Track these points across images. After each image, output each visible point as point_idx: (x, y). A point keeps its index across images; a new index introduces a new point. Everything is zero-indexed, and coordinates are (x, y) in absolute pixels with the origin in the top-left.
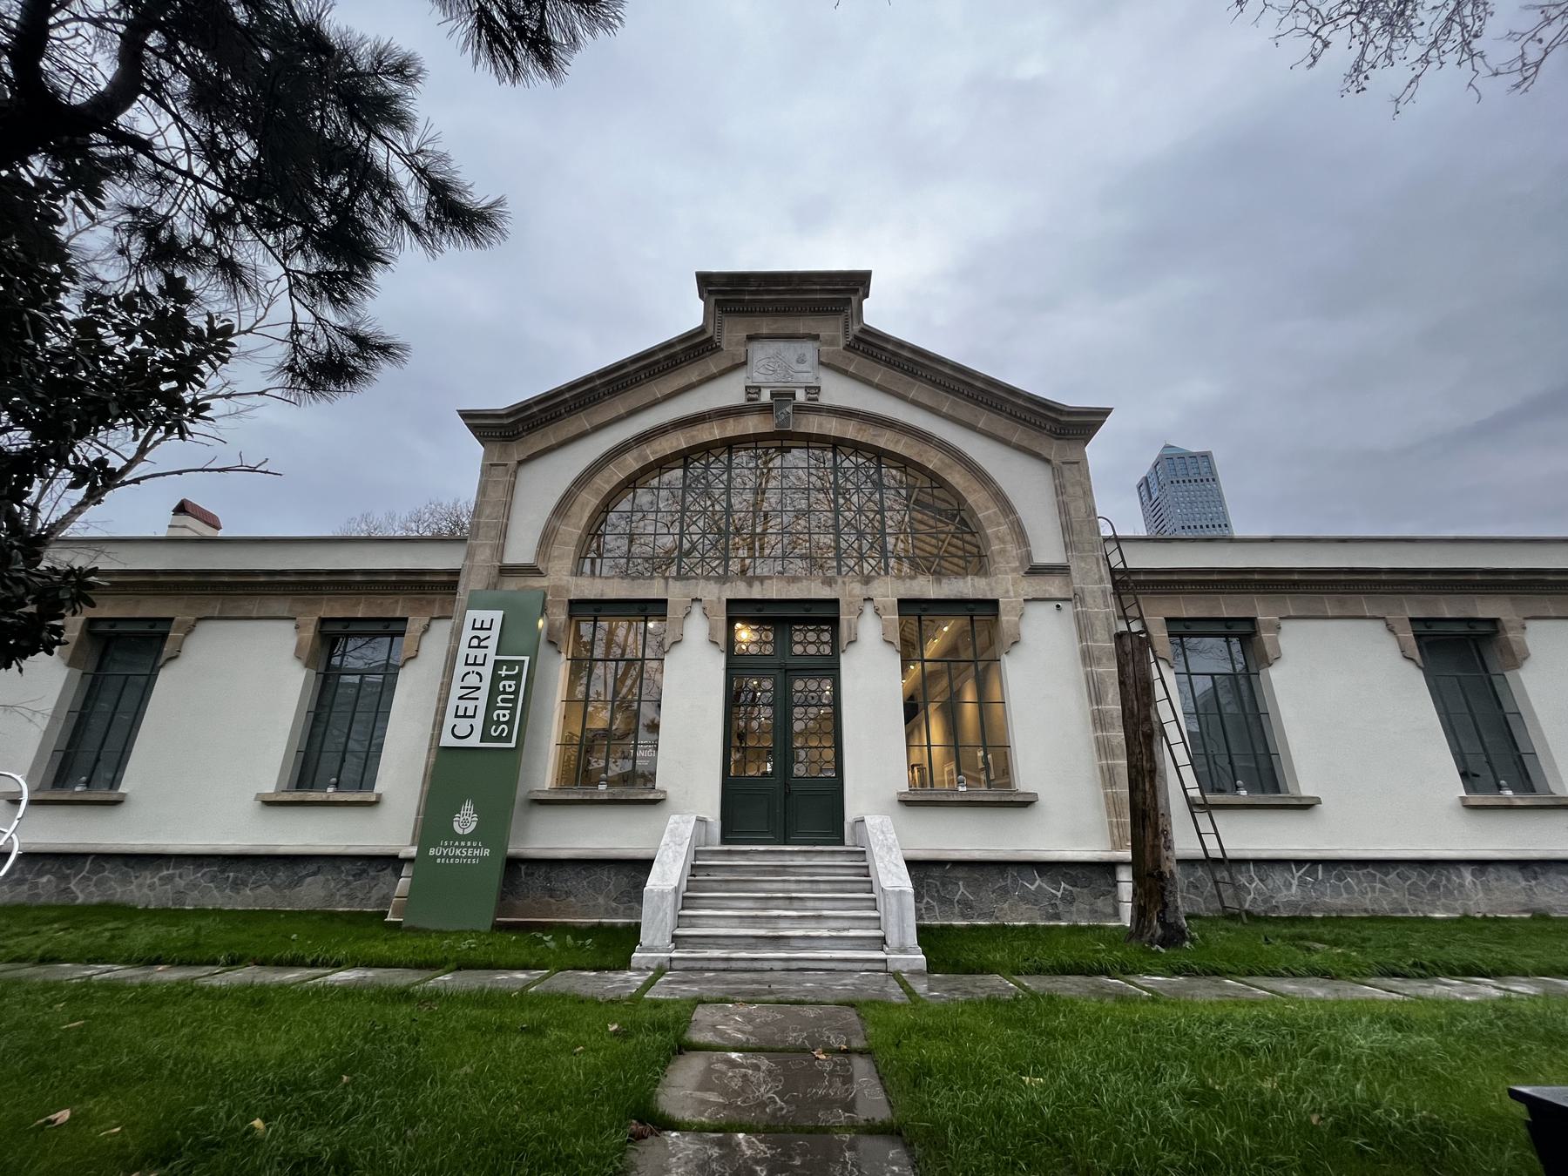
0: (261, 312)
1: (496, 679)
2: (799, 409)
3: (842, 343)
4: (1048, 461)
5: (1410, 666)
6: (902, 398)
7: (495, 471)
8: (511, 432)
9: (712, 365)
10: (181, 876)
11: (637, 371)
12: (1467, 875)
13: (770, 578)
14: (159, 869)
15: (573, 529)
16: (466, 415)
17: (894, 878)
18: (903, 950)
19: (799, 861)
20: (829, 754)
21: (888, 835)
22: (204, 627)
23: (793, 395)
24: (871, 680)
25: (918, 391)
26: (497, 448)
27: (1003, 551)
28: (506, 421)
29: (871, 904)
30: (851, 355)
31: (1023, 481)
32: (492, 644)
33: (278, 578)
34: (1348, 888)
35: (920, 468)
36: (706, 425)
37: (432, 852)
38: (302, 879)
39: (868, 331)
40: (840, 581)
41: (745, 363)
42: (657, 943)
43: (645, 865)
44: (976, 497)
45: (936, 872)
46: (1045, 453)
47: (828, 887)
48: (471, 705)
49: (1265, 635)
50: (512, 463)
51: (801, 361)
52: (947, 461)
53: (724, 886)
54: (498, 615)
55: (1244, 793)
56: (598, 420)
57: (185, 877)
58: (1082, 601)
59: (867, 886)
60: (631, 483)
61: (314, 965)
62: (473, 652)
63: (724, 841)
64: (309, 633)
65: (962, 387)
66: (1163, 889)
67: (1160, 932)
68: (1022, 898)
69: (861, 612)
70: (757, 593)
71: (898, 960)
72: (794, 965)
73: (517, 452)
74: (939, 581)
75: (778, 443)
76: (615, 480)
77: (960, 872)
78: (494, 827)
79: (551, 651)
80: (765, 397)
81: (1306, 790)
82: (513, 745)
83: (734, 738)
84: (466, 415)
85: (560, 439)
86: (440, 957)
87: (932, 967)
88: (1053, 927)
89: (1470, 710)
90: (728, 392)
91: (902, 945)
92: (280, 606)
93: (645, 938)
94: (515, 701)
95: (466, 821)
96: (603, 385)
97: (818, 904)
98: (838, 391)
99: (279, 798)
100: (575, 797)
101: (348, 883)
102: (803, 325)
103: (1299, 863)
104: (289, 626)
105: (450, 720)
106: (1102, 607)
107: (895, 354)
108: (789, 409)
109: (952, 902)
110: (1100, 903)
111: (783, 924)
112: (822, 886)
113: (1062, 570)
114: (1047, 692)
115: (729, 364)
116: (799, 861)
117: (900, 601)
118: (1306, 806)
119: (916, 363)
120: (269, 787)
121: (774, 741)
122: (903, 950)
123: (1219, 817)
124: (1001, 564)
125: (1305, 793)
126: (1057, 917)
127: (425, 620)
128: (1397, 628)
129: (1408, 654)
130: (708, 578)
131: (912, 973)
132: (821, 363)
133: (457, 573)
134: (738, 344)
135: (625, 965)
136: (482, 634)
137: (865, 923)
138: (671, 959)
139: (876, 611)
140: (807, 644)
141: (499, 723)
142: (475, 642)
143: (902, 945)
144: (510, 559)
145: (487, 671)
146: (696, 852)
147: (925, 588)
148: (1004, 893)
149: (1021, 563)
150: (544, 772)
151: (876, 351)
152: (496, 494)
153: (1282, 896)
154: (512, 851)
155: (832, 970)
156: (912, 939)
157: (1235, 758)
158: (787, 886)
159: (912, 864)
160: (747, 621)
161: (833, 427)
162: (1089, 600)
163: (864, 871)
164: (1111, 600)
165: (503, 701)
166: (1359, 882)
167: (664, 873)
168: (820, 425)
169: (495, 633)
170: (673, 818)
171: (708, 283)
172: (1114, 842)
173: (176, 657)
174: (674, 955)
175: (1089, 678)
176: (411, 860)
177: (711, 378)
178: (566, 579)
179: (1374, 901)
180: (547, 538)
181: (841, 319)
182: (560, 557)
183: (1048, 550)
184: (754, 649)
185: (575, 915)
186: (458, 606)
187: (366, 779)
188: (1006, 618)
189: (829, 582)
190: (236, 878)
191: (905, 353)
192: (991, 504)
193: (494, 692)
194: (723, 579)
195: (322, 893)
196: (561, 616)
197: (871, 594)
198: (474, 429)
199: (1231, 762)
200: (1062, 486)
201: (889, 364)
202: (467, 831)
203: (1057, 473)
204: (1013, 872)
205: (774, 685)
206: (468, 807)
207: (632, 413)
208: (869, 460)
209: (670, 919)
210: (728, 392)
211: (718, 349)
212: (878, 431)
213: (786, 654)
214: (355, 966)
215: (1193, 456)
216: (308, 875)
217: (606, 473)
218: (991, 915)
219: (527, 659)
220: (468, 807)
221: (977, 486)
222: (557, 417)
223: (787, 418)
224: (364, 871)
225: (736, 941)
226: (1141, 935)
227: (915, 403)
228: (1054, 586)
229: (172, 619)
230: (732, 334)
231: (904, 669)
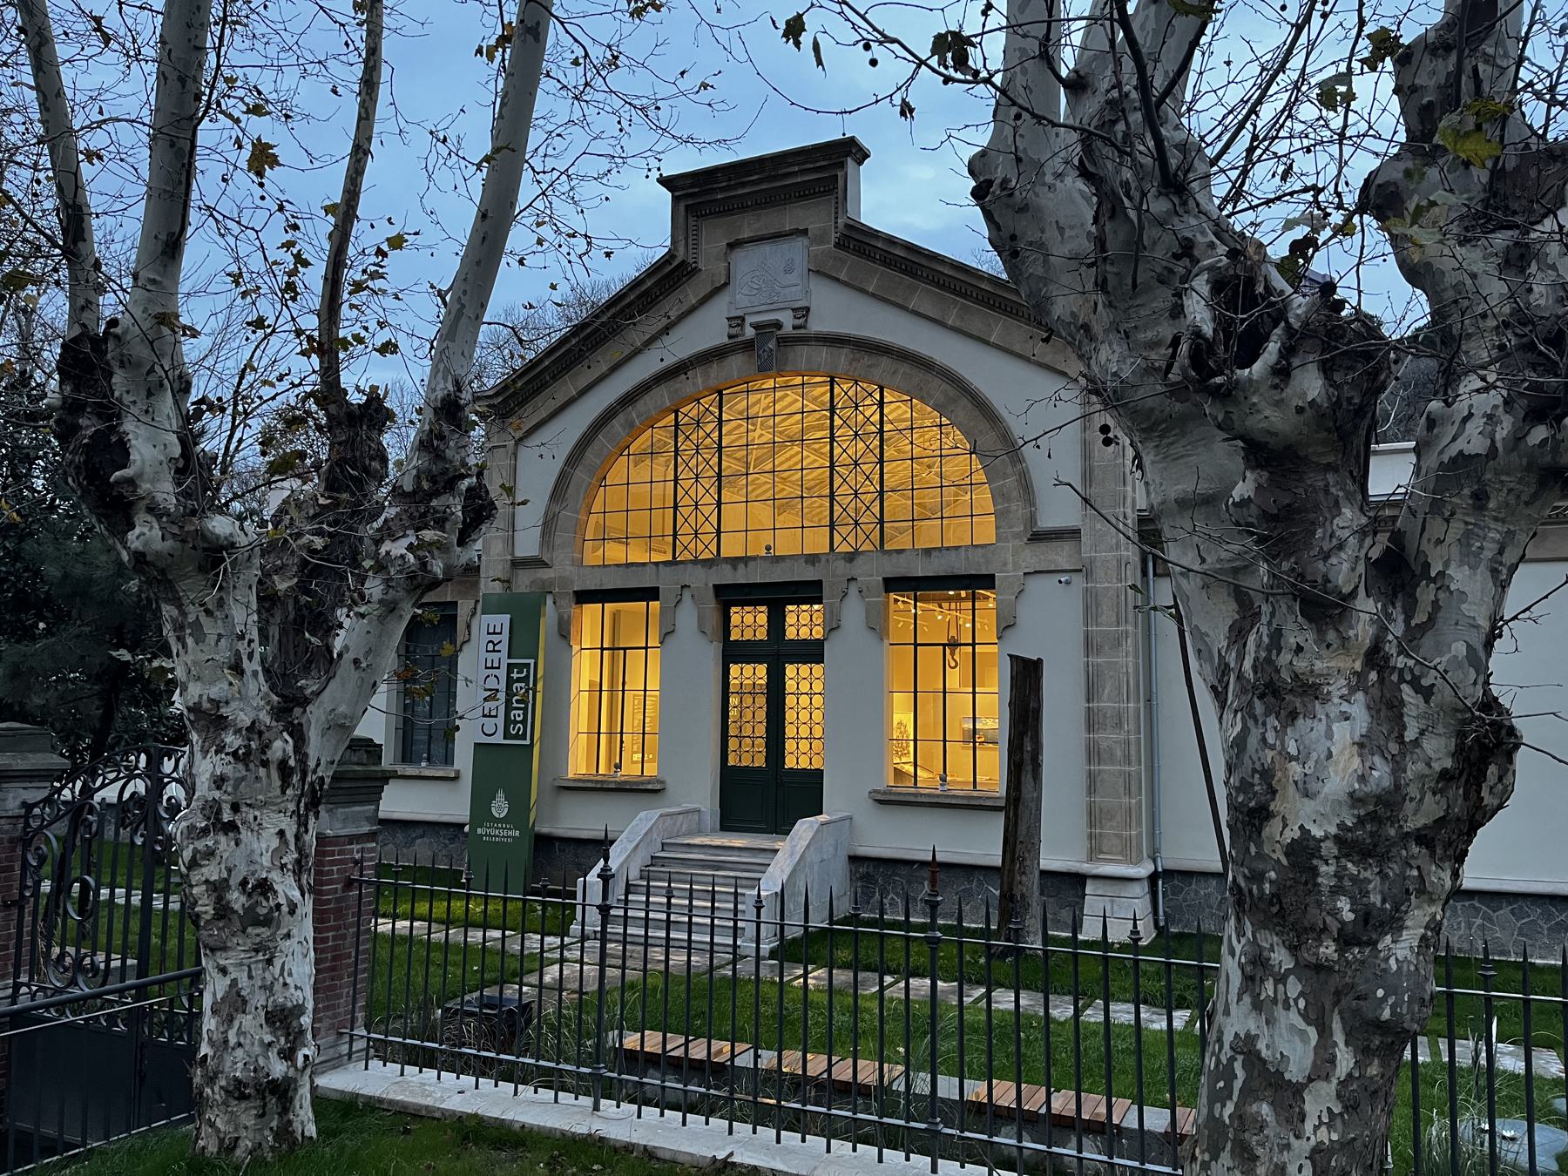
2: (785, 341)
3: (833, 238)
9: (691, 293)
25: (923, 298)
32: (504, 647)
45: (903, 871)
54: (505, 619)
56: (583, 382)
82: (528, 742)
90: (706, 330)
94: (527, 704)
95: (500, 807)
117: (886, 580)
136: (496, 638)
142: (490, 647)
162: (1099, 573)
193: (510, 694)
197: (854, 574)
206: (500, 795)
211: (696, 271)
219: (532, 661)
220: (500, 795)
228: (1060, 555)
230: (713, 240)
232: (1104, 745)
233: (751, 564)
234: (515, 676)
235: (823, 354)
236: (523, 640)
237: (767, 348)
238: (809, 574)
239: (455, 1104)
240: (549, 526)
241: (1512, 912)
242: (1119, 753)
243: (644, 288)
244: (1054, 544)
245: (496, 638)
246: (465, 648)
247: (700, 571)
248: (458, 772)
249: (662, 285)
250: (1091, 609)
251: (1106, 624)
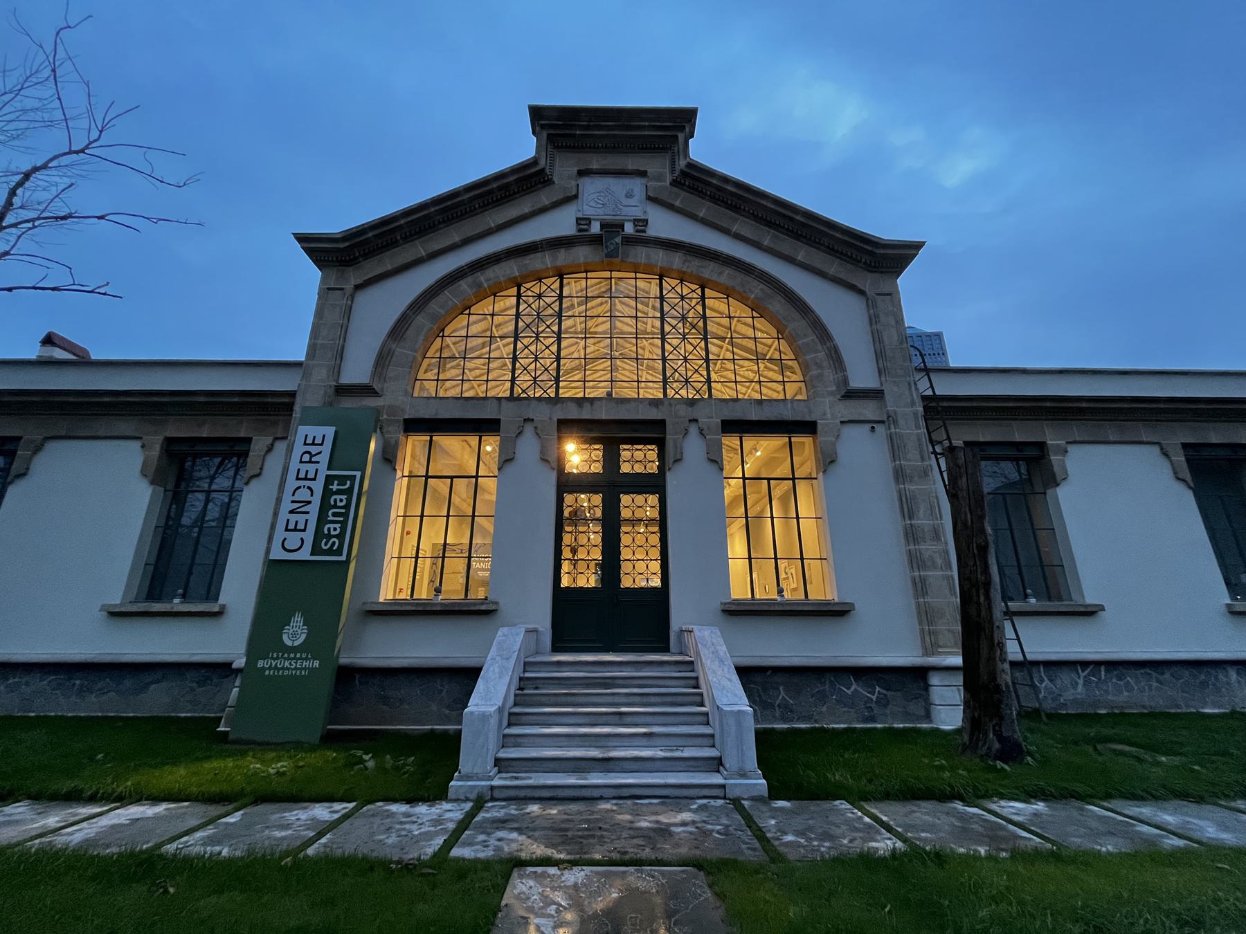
1: (327, 493)
2: (628, 240)
3: (669, 179)
4: (862, 292)
5: (1180, 488)
6: (725, 231)
9: (544, 197)
10: (27, 684)
12: (1233, 674)
16: (302, 239)
17: (729, 695)
22: (52, 446)
23: (622, 227)
28: (341, 246)
32: (324, 459)
36: (539, 255)
37: (260, 664)
39: (693, 166)
41: (576, 197)
43: (472, 674)
48: (301, 518)
49: (1054, 458)
50: (349, 287)
51: (629, 195)
54: (330, 431)
56: (436, 246)
58: (895, 422)
62: (304, 467)
64: (156, 451)
66: (1000, 702)
67: (997, 746)
69: (686, 432)
71: (736, 785)
73: (354, 277)
80: (596, 228)
82: (343, 558)
84: (302, 239)
87: (774, 793)
90: (561, 223)
91: (741, 769)
92: (124, 426)
93: (466, 762)
94: (346, 515)
95: (295, 633)
99: (123, 609)
102: (632, 163)
103: (1084, 664)
105: (280, 534)
106: (913, 429)
108: (618, 240)
109: (773, 706)
112: (653, 699)
115: (561, 196)
117: (723, 422)
118: (1089, 612)
119: (740, 197)
120: (116, 598)
122: (743, 775)
123: (1020, 622)
125: (1089, 601)
126: (872, 719)
127: (269, 440)
132: (649, 198)
133: (292, 394)
134: (569, 178)
137: (698, 741)
138: (492, 788)
139: (701, 432)
140: (638, 459)
141: (329, 536)
143: (741, 769)
144: (346, 379)
145: (318, 486)
149: (838, 386)
153: (1069, 695)
154: (344, 660)
157: (1024, 569)
158: (616, 699)
159: (745, 673)
162: (901, 422)
164: (922, 423)
165: (334, 515)
168: (648, 257)
171: (538, 114)
172: (925, 648)
173: (24, 474)
174: (496, 783)
176: (239, 671)
183: (862, 375)
186: (294, 422)
187: (212, 590)
190: (82, 686)
197: (695, 416)
198: (310, 252)
199: (1020, 573)
200: (877, 316)
201: (714, 199)
202: (296, 643)
203: (870, 303)
206: (298, 620)
207: (466, 242)
209: (493, 740)
215: (929, 335)
216: (152, 683)
218: (808, 718)
219: (358, 474)
220: (298, 620)
222: (393, 244)
227: (738, 237)
228: (868, 410)
229: (19, 438)
230: (563, 170)
232: (926, 555)
233: (597, 404)
234: (335, 487)
235: (660, 257)
236: (346, 453)
237: (611, 245)
238: (654, 414)
239: (77, 836)
240: (383, 360)
241: (1172, 675)
244: (862, 402)
246: (254, 483)
247: (545, 408)
248: (223, 607)
249: (517, 185)
251: (912, 460)
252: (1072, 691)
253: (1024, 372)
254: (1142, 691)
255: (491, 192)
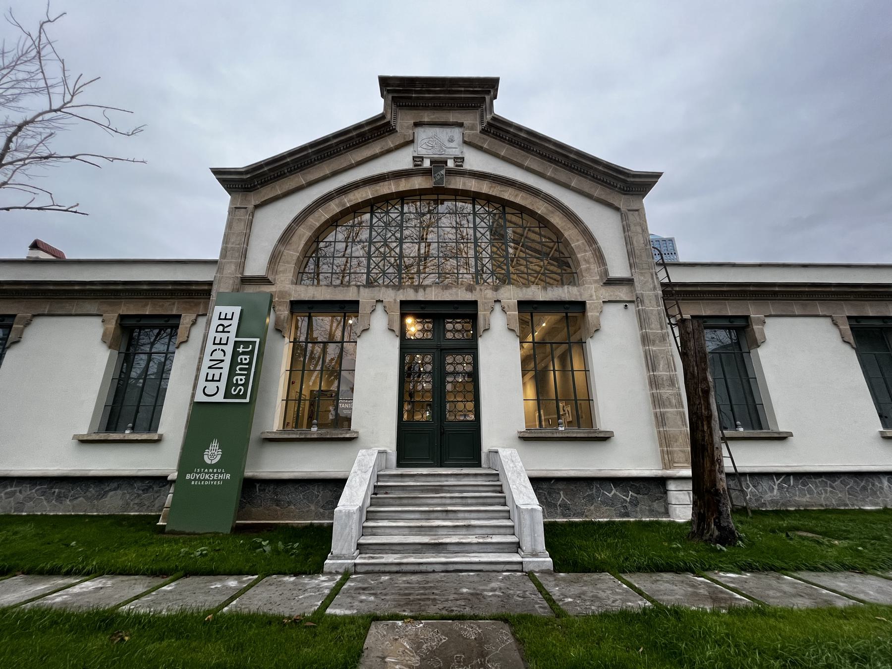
0: (68, 98)
1: (235, 354)
2: (450, 172)
3: (479, 128)
4: (617, 209)
5: (847, 348)
7: (238, 212)
8: (249, 185)
9: (390, 142)
10: (20, 492)
11: (337, 144)
13: (430, 286)
14: (5, 487)
15: (294, 252)
17: (524, 497)
18: (535, 554)
19: (452, 482)
20: (470, 405)
21: (516, 466)
23: (446, 163)
24: (500, 357)
25: (531, 161)
26: (239, 197)
27: (588, 269)
28: (245, 177)
29: (506, 515)
30: (485, 137)
31: (602, 223)
32: (233, 329)
33: (88, 287)
34: (810, 492)
35: (532, 213)
36: (386, 183)
37: (188, 477)
38: (106, 493)
39: (496, 119)
40: (478, 288)
41: (412, 142)
42: (344, 552)
43: (339, 484)
44: (570, 233)
46: (616, 204)
47: (474, 501)
48: (217, 372)
51: (451, 140)
52: (550, 208)
53: (398, 502)
54: (237, 310)
55: (741, 429)
57: (23, 493)
58: (642, 302)
59: (502, 500)
60: (333, 222)
61: (68, 574)
62: (219, 335)
63: (399, 465)
64: (112, 325)
65: (560, 158)
66: (719, 501)
67: (717, 533)
68: (603, 503)
69: (493, 309)
70: (421, 296)
72: (451, 568)
73: (254, 199)
74: (545, 288)
75: (435, 197)
76: (323, 219)
77: (560, 486)
78: (234, 457)
79: (278, 336)
80: (427, 164)
81: (782, 428)
82: (247, 400)
83: (405, 395)
85: (284, 190)
86: (173, 566)
87: (558, 567)
88: (625, 522)
89: (883, 375)
90: (402, 160)
91: (534, 550)
94: (249, 370)
95: (213, 454)
96: (315, 153)
97: (467, 515)
98: (475, 161)
100: (294, 436)
101: (139, 495)
102: (452, 117)
103: (778, 475)
104: (97, 321)
105: (202, 383)
106: (654, 307)
107: (515, 135)
108: (443, 172)
109: (555, 506)
110: (655, 505)
111: (441, 532)
112: (470, 501)
113: (628, 282)
114: (622, 367)
115: (402, 141)
116: (452, 482)
118: (782, 438)
119: (530, 141)
120: (83, 430)
121: (433, 397)
124: (588, 278)
125: (782, 429)
126: (627, 515)
127: (194, 316)
128: (839, 322)
129: (846, 339)
130: (387, 286)
131: (542, 572)
132: (465, 142)
133: (210, 284)
134: (408, 128)
135: (319, 569)
136: (226, 323)
138: (355, 565)
140: (453, 329)
141: (237, 385)
142: (220, 329)
143: (534, 550)
144: (248, 273)
145: (229, 349)
146: (378, 476)
147: (536, 293)
148: (591, 499)
149: (601, 277)
150: (273, 419)
151: (502, 133)
152: (240, 227)
153: (768, 497)
154: (249, 473)
155: (485, 571)
156: (541, 546)
158: (444, 501)
160: (417, 316)
161: (472, 185)
162: (646, 302)
163: (498, 489)
164: (661, 302)
165: (241, 369)
166: (817, 487)
167: (352, 495)
168: (464, 184)
169: (235, 322)
170: (362, 452)
174: (358, 561)
175: (647, 354)
177: (389, 151)
178: (287, 287)
179: (826, 499)
180: (275, 258)
181: (478, 113)
182: (284, 272)
183: (618, 268)
184: (419, 336)
185: (294, 518)
186: (211, 303)
187: (152, 424)
188: (591, 314)
189: (470, 289)
190: (60, 492)
191: (523, 135)
192: (580, 237)
194: (399, 287)
195: (121, 503)
196: (285, 312)
198: (222, 181)
199: (732, 410)
200: (628, 226)
201: (511, 143)
203: (624, 217)
204: (596, 485)
205: (445, 335)
206: (215, 445)
208: (497, 209)
209: (355, 530)
210: (402, 160)
211: (393, 131)
212: (504, 188)
213: (442, 342)
214: (101, 575)
216: (111, 490)
217: (316, 214)
218: (581, 514)
219: (258, 340)
220: (215, 445)
221: (570, 225)
223: (442, 179)
224: (150, 487)
225: (406, 547)
226: (702, 534)
228: (622, 293)
229: (15, 316)
230: (404, 122)
231: (522, 347)
232: (665, 397)
234: (241, 350)
242: (674, 401)
243: (363, 130)
245: (226, 323)
246: (183, 347)
250: (642, 320)
252: (770, 494)
253: (734, 265)
254: (819, 494)
255: (351, 138)
